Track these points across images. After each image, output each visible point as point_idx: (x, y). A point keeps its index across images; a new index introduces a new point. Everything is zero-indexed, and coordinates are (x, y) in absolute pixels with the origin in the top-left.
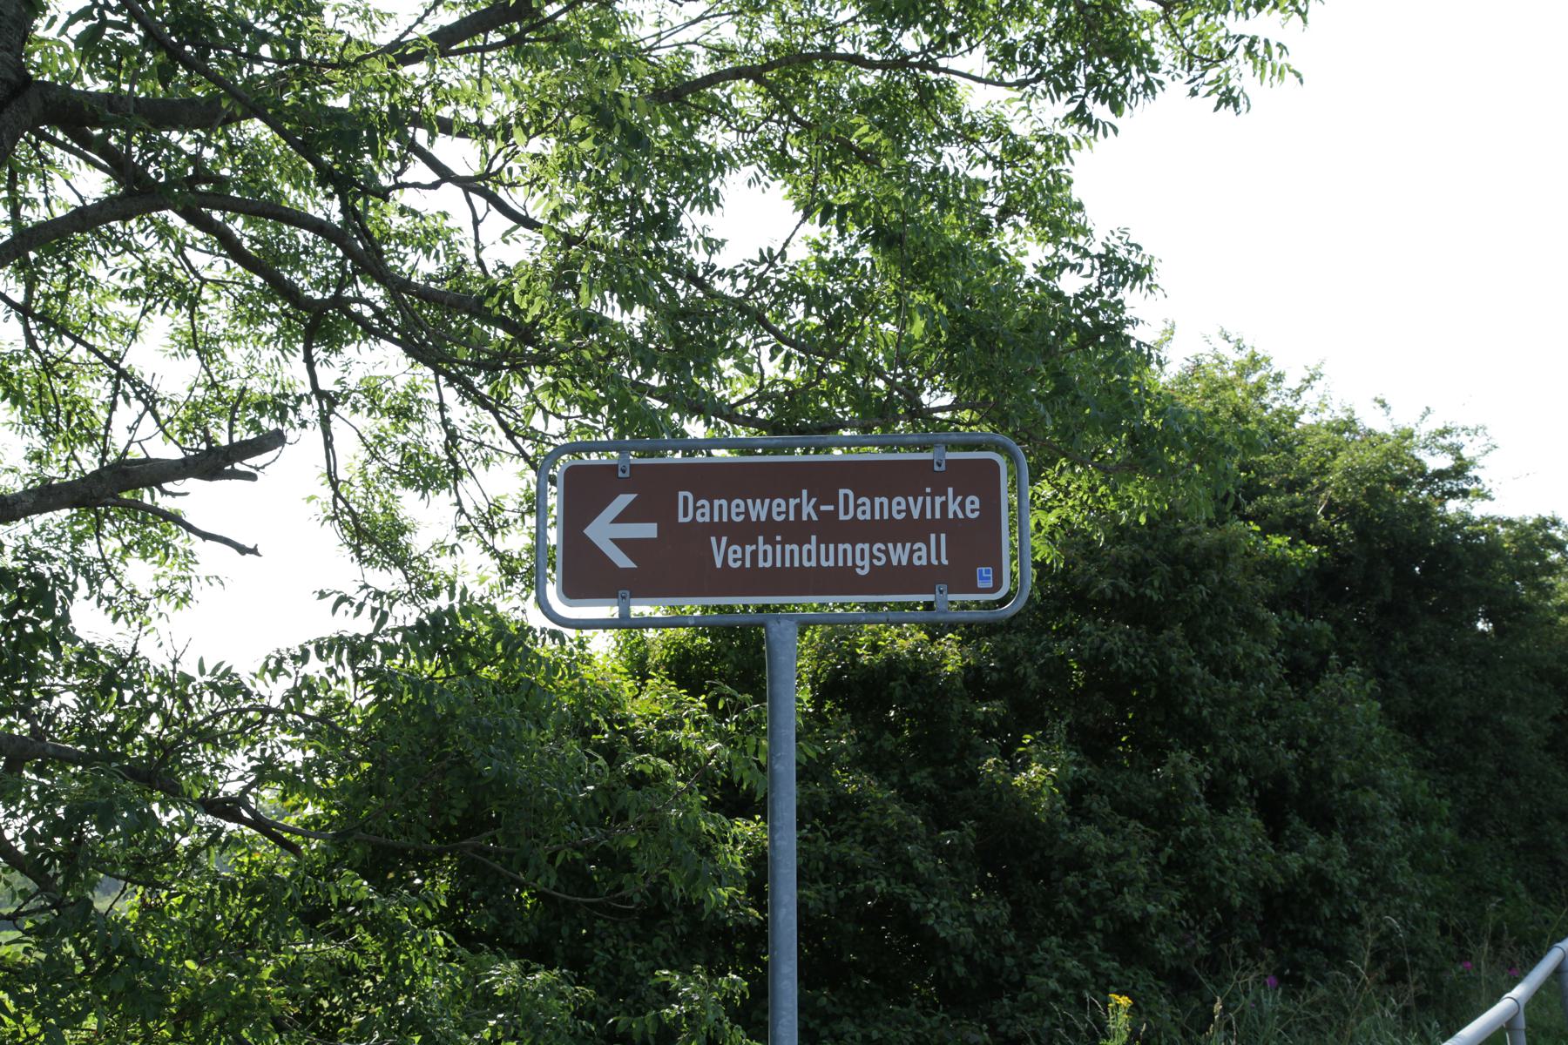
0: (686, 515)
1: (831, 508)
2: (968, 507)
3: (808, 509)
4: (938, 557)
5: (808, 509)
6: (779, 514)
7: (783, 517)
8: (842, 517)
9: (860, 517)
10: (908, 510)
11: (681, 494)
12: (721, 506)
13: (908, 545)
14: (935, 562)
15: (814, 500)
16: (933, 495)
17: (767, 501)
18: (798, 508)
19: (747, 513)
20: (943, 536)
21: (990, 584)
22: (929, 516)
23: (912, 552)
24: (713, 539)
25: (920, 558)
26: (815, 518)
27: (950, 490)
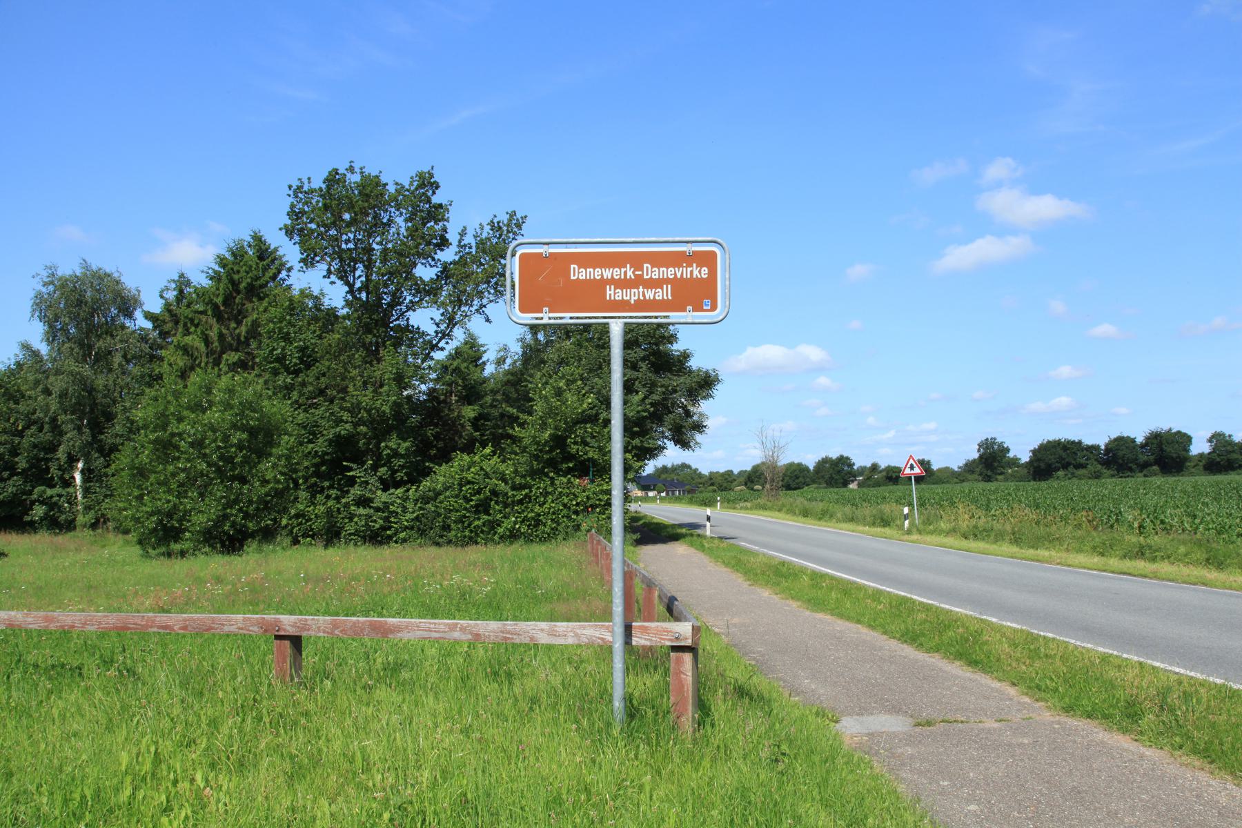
3: (630, 274)
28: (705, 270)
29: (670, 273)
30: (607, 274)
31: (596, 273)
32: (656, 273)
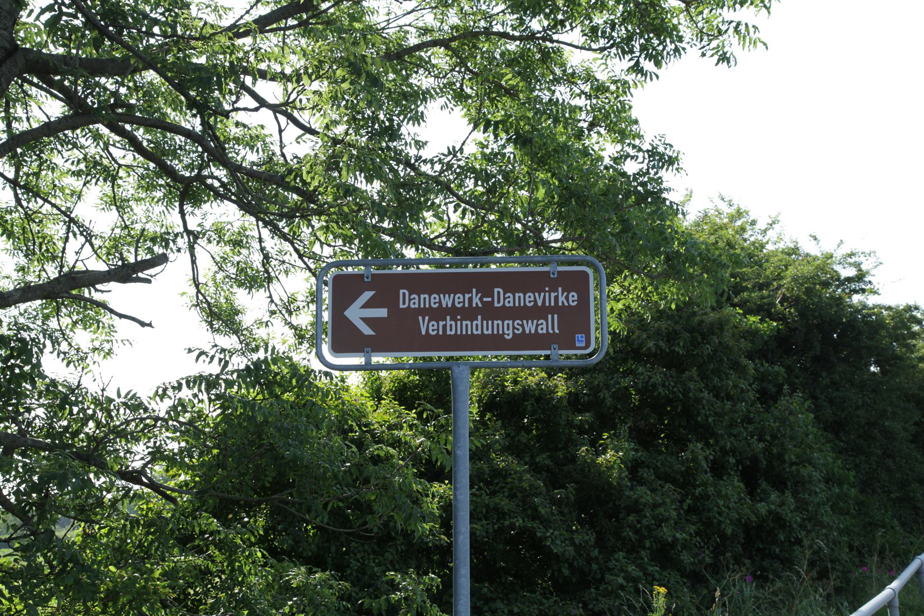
0: (404, 303)
1: (490, 299)
2: (571, 299)
3: (476, 300)
4: (553, 328)
5: (476, 300)
6: (459, 303)
7: (461, 305)
8: (496, 305)
9: (507, 305)
10: (535, 301)
11: (401, 291)
12: (425, 299)
13: (535, 321)
14: (551, 331)
15: (479, 295)
16: (550, 292)
17: (452, 295)
18: (470, 299)
19: (440, 302)
20: (556, 316)
21: (583, 345)
22: (547, 304)
23: (537, 325)
24: (420, 318)
25: (542, 329)
26: (480, 305)
27: (560, 289)
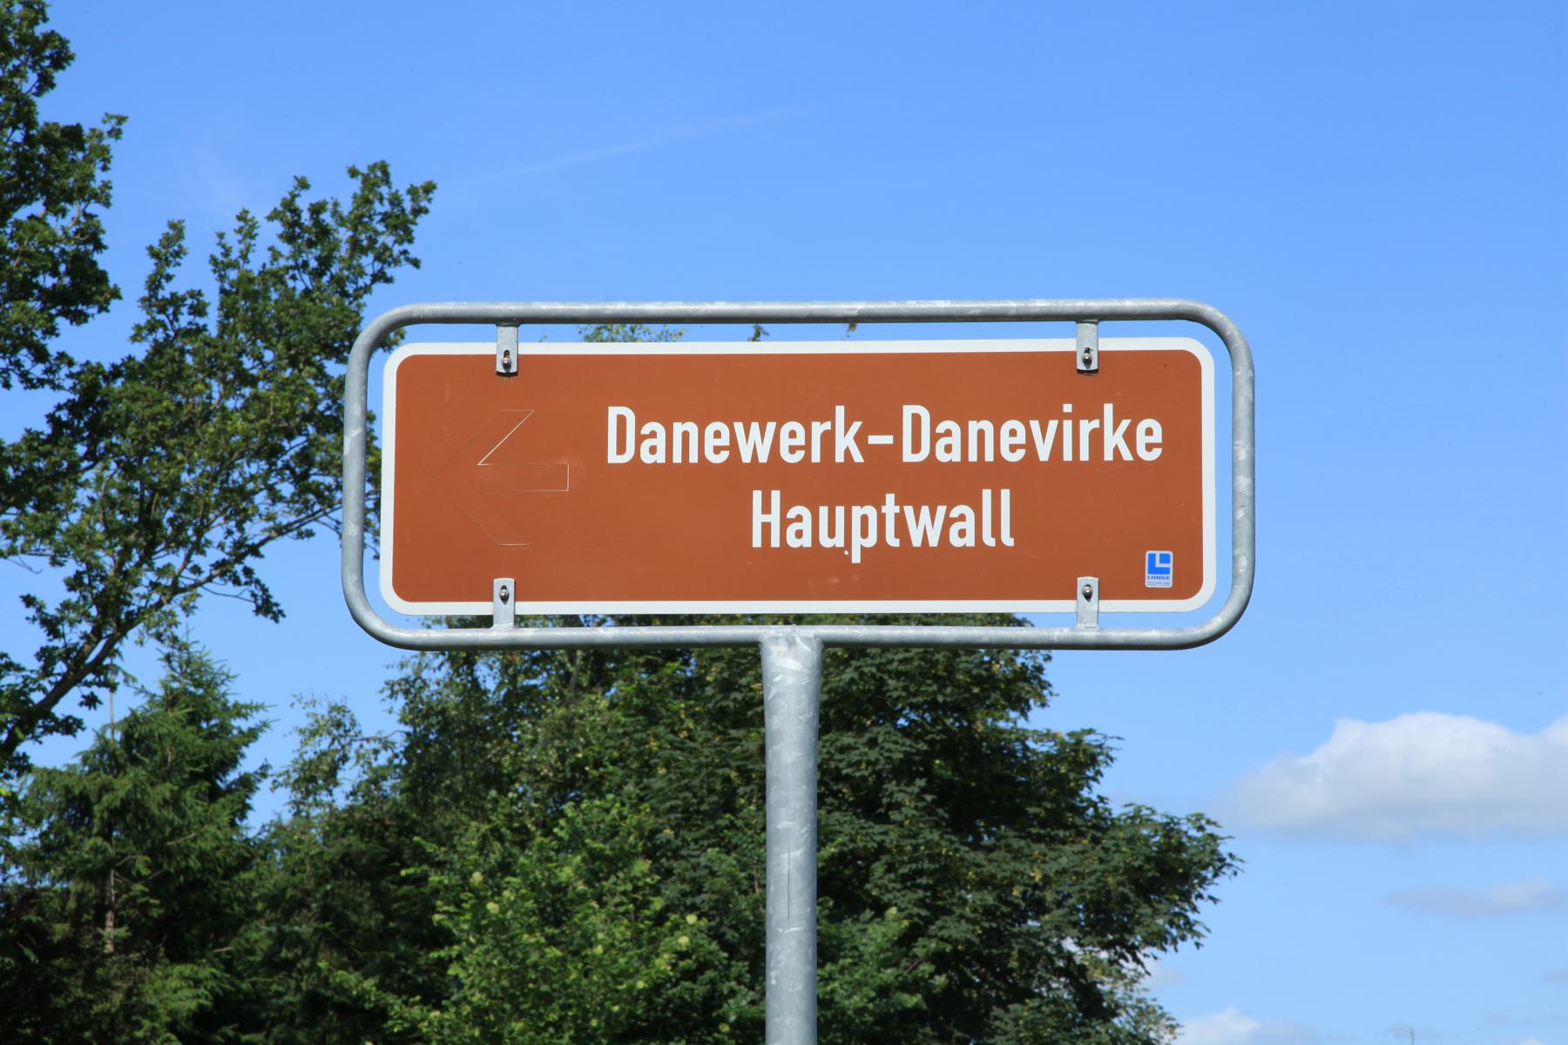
0: (621, 449)
1: (888, 440)
2: (1142, 440)
3: (845, 442)
4: (996, 532)
5: (845, 442)
6: (793, 450)
7: (800, 455)
8: (908, 456)
9: (942, 456)
10: (1030, 445)
11: (614, 412)
12: (981, 434)
13: (941, 510)
14: (990, 541)
15: (856, 426)
16: (1076, 417)
17: (771, 426)
18: (828, 439)
19: (733, 447)
20: (1005, 494)
21: (1167, 582)
22: (1068, 456)
23: (948, 522)
24: (757, 496)
25: (962, 533)
26: (858, 457)
27: (1108, 409)
28: (1151, 431)
29: (1009, 439)
30: (755, 443)
31: (710, 442)
32: (950, 443)
